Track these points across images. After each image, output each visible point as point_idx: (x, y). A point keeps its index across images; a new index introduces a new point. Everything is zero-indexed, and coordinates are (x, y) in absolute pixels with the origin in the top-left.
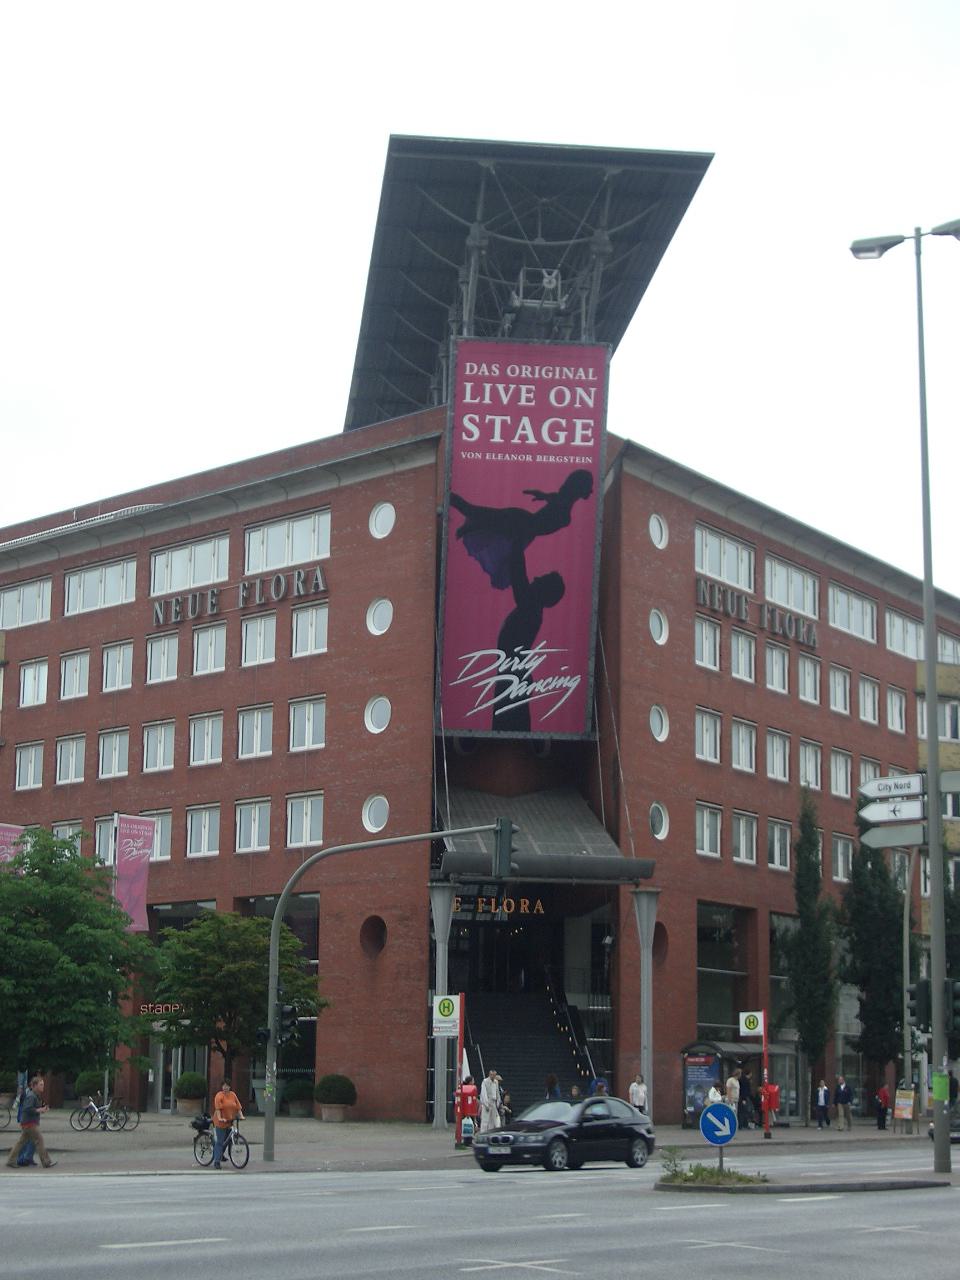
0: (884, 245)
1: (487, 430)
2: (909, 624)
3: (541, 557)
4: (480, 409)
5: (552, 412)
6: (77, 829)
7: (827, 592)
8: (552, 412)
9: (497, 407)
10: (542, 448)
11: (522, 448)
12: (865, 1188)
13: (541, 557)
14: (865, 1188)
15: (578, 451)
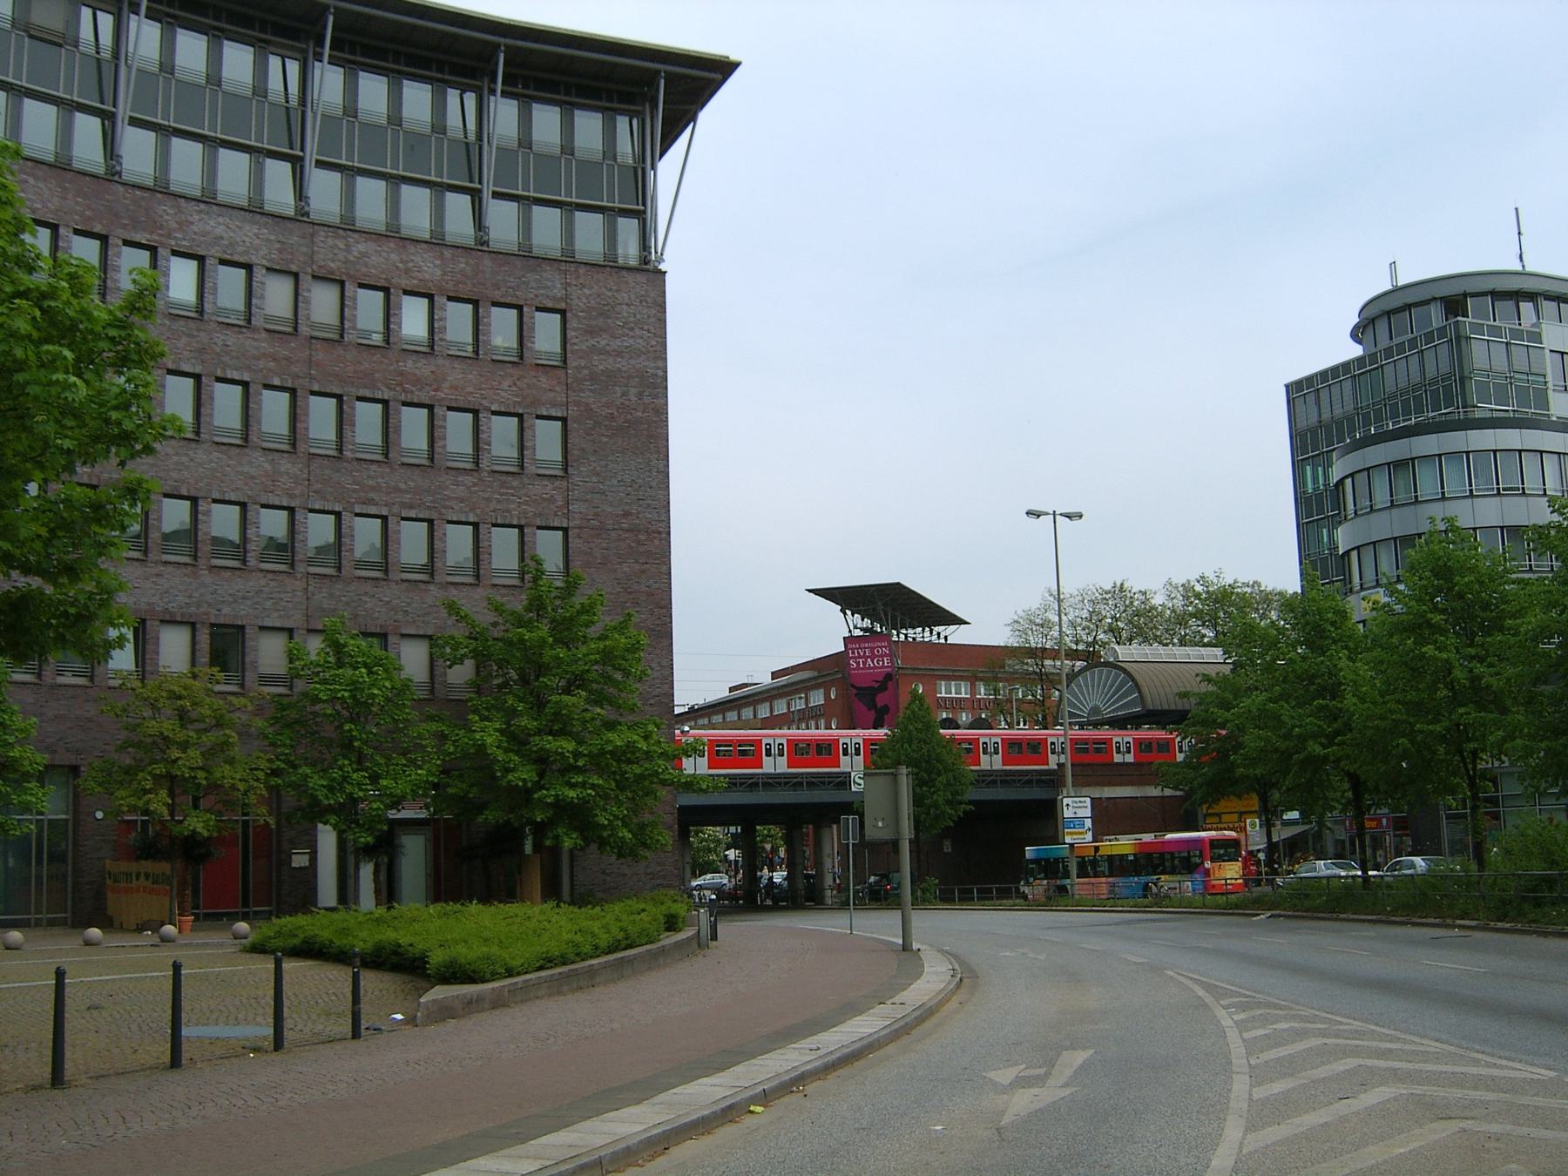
0: (1038, 515)
1: (858, 664)
2: (1167, 708)
3: (881, 700)
4: (855, 658)
5: (876, 656)
6: (504, 783)
7: (724, 824)
8: (876, 656)
9: (860, 657)
10: (875, 667)
11: (870, 668)
12: (289, 124)
13: (881, 700)
14: (289, 124)
15: (888, 667)
